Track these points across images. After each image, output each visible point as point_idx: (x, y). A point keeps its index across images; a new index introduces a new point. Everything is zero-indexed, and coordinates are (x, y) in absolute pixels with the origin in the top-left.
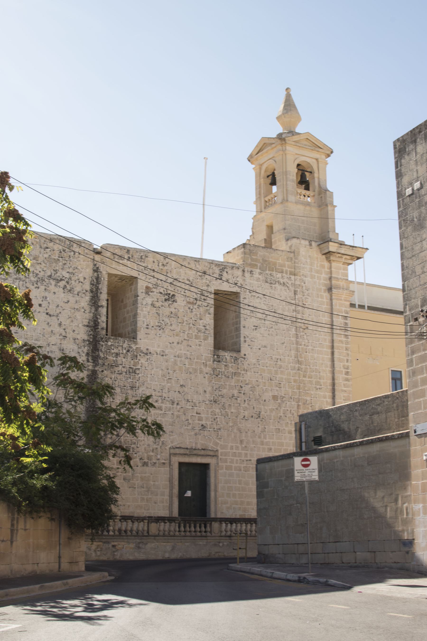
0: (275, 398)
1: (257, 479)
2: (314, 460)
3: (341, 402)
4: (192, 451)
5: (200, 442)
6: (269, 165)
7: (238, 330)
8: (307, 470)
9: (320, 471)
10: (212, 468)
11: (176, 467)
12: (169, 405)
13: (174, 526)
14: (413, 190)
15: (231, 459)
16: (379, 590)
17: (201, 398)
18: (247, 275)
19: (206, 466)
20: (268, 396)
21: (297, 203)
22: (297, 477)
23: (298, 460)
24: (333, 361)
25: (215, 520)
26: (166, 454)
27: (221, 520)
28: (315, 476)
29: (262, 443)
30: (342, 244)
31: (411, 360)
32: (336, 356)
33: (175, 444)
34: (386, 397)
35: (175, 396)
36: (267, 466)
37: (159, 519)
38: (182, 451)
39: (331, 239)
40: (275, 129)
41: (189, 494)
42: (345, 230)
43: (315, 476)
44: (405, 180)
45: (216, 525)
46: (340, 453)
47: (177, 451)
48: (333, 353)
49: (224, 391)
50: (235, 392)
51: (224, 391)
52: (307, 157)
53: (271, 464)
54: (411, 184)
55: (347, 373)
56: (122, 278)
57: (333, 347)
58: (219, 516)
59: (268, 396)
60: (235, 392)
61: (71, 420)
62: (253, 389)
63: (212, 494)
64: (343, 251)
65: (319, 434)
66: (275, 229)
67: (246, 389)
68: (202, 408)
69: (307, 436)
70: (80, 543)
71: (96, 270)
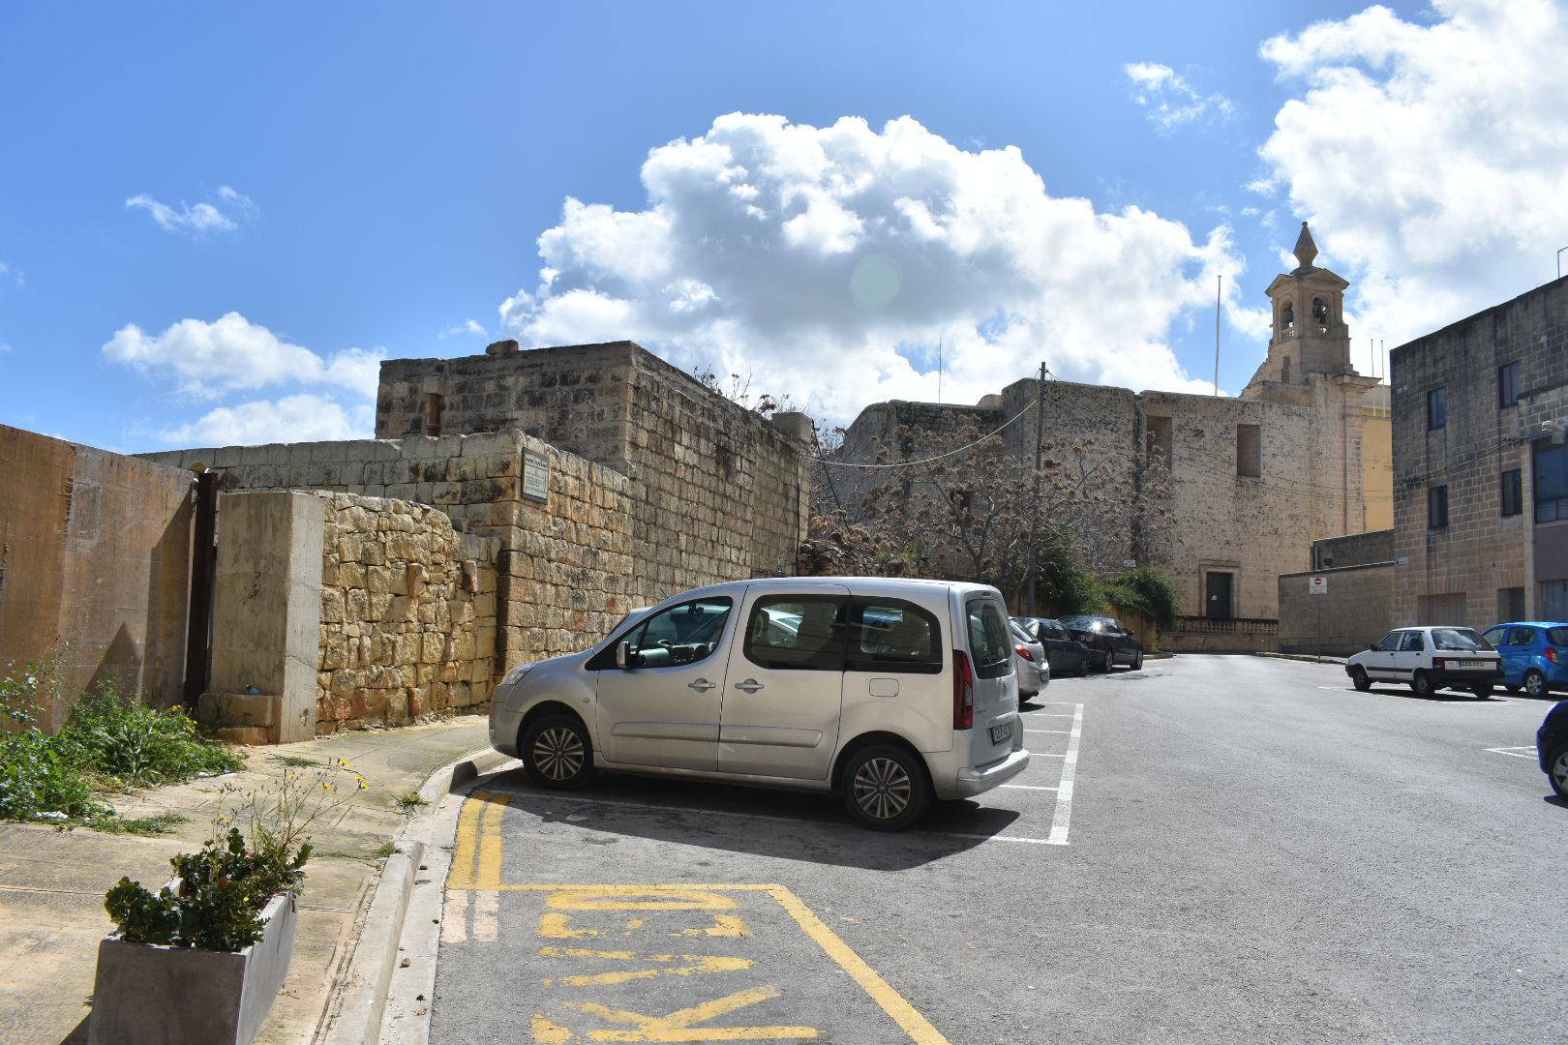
0: (1291, 517)
3: (513, 581)
4: (1218, 563)
5: (1226, 554)
6: (1284, 299)
7: (1258, 458)
8: (1319, 586)
13: (1204, 624)
14: (729, 912)
15: (1413, 633)
19: (1230, 575)
20: (1284, 515)
22: (1312, 591)
23: (1312, 580)
30: (1355, 375)
35: (1202, 516)
37: (1192, 619)
40: (1292, 263)
45: (1239, 625)
46: (1345, 575)
52: (1323, 290)
56: (1158, 419)
59: (1284, 515)
61: (413, 391)
67: (1266, 509)
71: (1138, 414)
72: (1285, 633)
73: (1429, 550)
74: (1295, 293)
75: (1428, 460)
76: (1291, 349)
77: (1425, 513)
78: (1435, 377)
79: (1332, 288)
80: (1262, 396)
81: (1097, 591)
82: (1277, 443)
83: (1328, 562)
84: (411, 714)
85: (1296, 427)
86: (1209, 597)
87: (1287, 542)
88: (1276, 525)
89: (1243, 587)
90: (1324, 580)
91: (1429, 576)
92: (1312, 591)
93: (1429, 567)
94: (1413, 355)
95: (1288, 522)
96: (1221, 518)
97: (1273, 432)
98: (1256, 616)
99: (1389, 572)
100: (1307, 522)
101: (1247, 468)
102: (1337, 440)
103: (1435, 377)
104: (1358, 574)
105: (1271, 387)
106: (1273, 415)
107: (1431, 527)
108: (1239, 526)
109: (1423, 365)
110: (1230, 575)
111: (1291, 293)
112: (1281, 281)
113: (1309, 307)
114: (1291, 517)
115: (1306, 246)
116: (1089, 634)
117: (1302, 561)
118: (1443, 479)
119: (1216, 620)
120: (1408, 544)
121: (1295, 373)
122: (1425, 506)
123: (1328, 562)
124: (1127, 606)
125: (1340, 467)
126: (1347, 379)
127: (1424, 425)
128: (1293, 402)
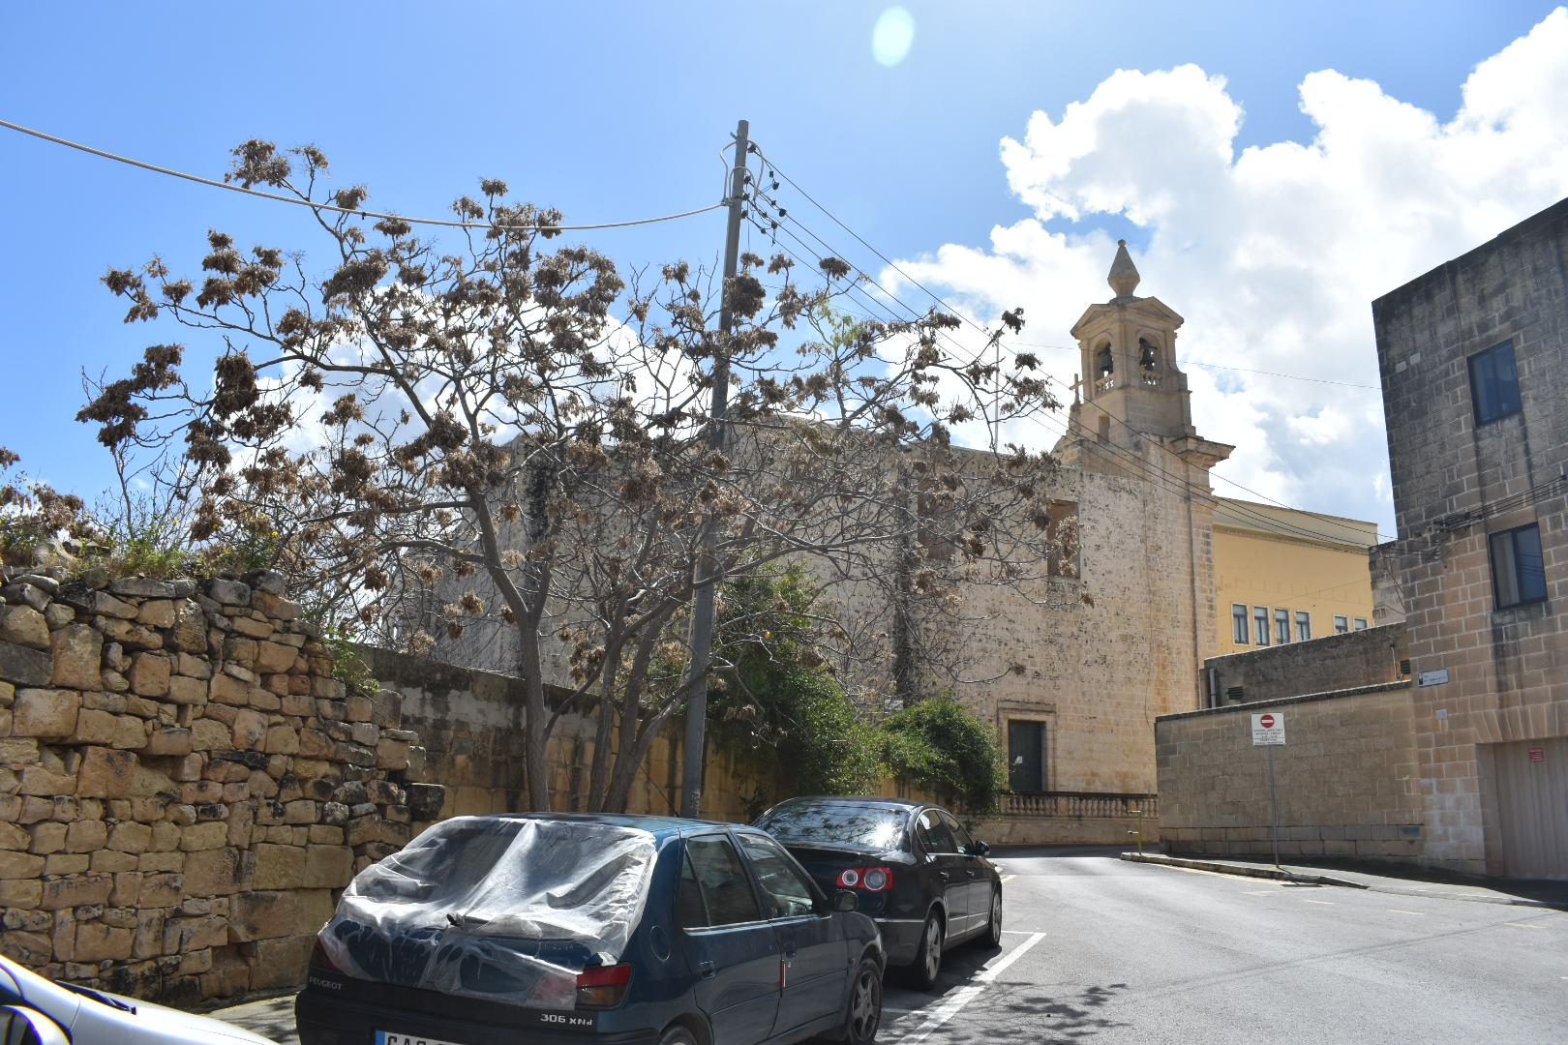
0: (1124, 638)
1: (1157, 742)
2: (1278, 718)
4: (1023, 706)
5: (1035, 693)
6: (1098, 338)
9: (1287, 731)
10: (1049, 726)
11: (1005, 724)
12: (995, 646)
16: (706, 845)
17: (1034, 637)
18: (1086, 480)
19: (1041, 725)
20: (1113, 635)
21: (1142, 388)
22: (1257, 740)
24: (1193, 592)
25: (1057, 794)
26: (992, 710)
27: (1068, 795)
28: (1281, 739)
29: (1109, 696)
30: (1200, 440)
31: (1412, 588)
32: (1197, 584)
33: (1003, 695)
34: (1328, 639)
36: (1174, 725)
38: (1012, 705)
39: (1420, 413)
40: (1107, 294)
41: (1019, 760)
42: (1303, 418)
43: (1281, 739)
44: (1394, 352)
45: (1062, 801)
47: (1007, 705)
48: (1193, 581)
49: (1061, 629)
50: (1075, 630)
51: (1061, 629)
52: (1152, 327)
53: (1182, 723)
54: (1405, 357)
55: (1211, 607)
57: (1192, 573)
58: (1060, 789)
59: (1113, 635)
60: (1075, 630)
62: (1096, 626)
63: (1050, 761)
64: (1203, 449)
65: (1237, 685)
66: (1112, 421)
67: (1089, 625)
68: (1035, 650)
69: (1218, 687)
70: (1488, 853)
72: (1144, 821)
73: (1499, 652)
74: (1116, 328)
75: (1481, 481)
76: (1112, 403)
77: (1485, 581)
78: (1484, 327)
79: (1161, 325)
80: (1080, 460)
81: (865, 740)
82: (1102, 531)
83: (1236, 694)
84: (1497, 674)
85: (1125, 507)
86: (1012, 759)
87: (1119, 676)
88: (1104, 649)
89: (1061, 742)
90: (1278, 718)
91: (1503, 703)
92: (1257, 740)
93: (1501, 687)
94: (1429, 297)
95: (1120, 647)
96: (1028, 637)
97: (1096, 514)
98: (1081, 787)
99: (1404, 701)
100: (1144, 647)
101: (1062, 563)
102: (1179, 529)
103: (1484, 327)
104: (1325, 708)
105: (1088, 441)
106: (1092, 491)
107: (1499, 607)
108: (1053, 651)
109: (1453, 310)
110: (1040, 726)
111: (1109, 330)
112: (1095, 313)
113: (1135, 349)
114: (1124, 638)
115: (1123, 274)
116: (868, 862)
117: (1185, 699)
118: (1525, 512)
119: (1027, 795)
120: (1446, 645)
121: (1118, 434)
122: (1483, 569)
123: (1236, 694)
124: (916, 772)
125: (1186, 568)
126: (1191, 444)
127: (1466, 419)
128: (1120, 471)
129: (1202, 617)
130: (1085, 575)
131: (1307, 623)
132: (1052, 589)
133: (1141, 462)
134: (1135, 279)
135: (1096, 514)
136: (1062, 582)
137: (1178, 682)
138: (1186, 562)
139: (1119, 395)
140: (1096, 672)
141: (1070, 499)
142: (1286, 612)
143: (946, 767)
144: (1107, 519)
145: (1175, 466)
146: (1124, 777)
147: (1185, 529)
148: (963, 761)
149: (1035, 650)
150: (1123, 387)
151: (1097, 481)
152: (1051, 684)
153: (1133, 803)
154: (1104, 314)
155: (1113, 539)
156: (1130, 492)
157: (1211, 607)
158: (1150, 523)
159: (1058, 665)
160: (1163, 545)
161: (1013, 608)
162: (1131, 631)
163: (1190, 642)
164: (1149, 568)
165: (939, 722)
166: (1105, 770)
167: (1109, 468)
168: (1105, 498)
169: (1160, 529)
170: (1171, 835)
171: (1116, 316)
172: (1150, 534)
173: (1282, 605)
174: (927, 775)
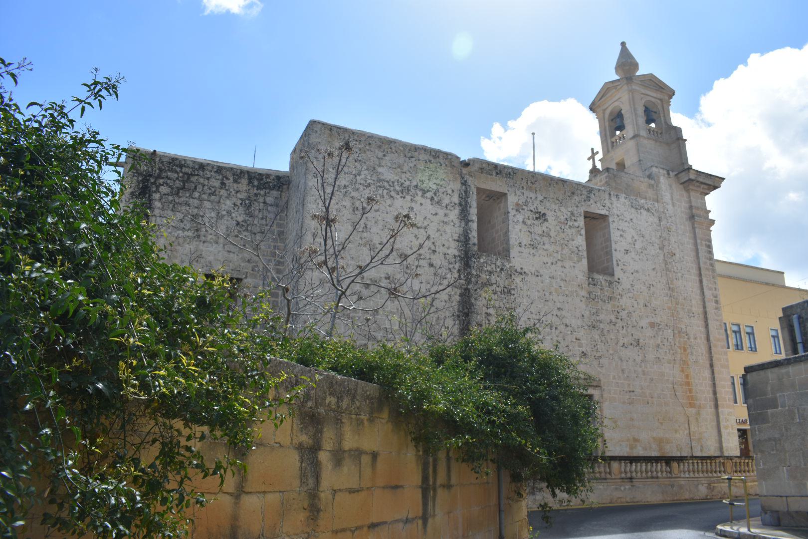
10: (596, 398)
17: (579, 322)
18: (614, 199)
29: (644, 373)
45: (615, 465)
48: (701, 281)
49: (602, 317)
50: (613, 318)
57: (700, 275)
59: (644, 323)
60: (613, 318)
62: (629, 314)
67: (624, 314)
68: (581, 334)
76: (628, 152)
82: (629, 239)
85: (645, 221)
87: (651, 356)
95: (649, 332)
96: (575, 323)
98: (624, 451)
108: (596, 334)
112: (608, 89)
114: (652, 325)
124: (451, 425)
125: (694, 271)
128: (638, 194)
129: (710, 306)
130: (618, 273)
131: (753, 334)
132: (593, 283)
133: (655, 187)
134: (635, 66)
135: (623, 225)
136: (600, 278)
137: (696, 362)
138: (695, 266)
139: (631, 144)
140: (632, 353)
141: (603, 212)
142: (739, 325)
143: (514, 418)
144: (631, 228)
145: (679, 193)
146: (660, 441)
147: (692, 241)
148: (537, 408)
149: (581, 334)
150: (635, 137)
151: (622, 200)
152: (595, 363)
153: (675, 465)
154: (615, 87)
155: (638, 245)
156: (648, 210)
157: (717, 302)
158: (665, 235)
159: (600, 346)
160: (677, 251)
161: (561, 298)
162: (657, 320)
163: (703, 329)
164: (667, 270)
165: (497, 350)
166: (644, 436)
167: (630, 191)
168: (630, 214)
169: (673, 240)
170: (779, 505)
171: (625, 87)
172: (666, 243)
173: (735, 322)
174: (471, 430)
